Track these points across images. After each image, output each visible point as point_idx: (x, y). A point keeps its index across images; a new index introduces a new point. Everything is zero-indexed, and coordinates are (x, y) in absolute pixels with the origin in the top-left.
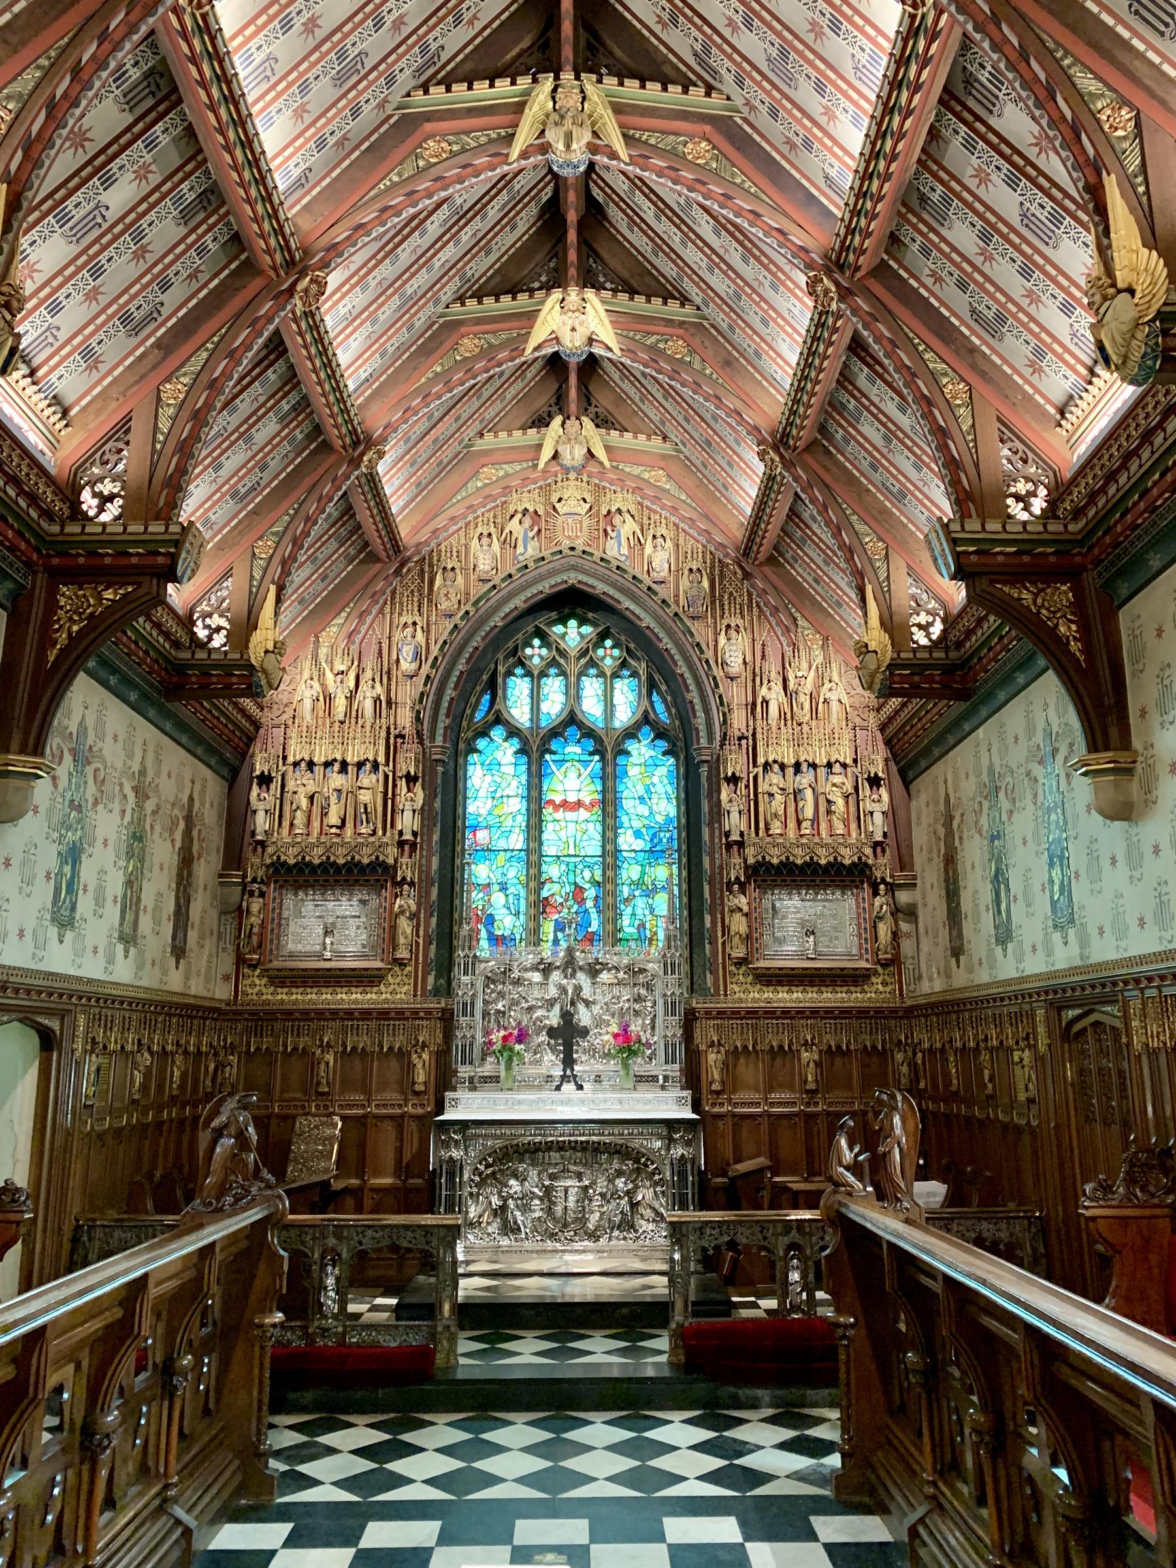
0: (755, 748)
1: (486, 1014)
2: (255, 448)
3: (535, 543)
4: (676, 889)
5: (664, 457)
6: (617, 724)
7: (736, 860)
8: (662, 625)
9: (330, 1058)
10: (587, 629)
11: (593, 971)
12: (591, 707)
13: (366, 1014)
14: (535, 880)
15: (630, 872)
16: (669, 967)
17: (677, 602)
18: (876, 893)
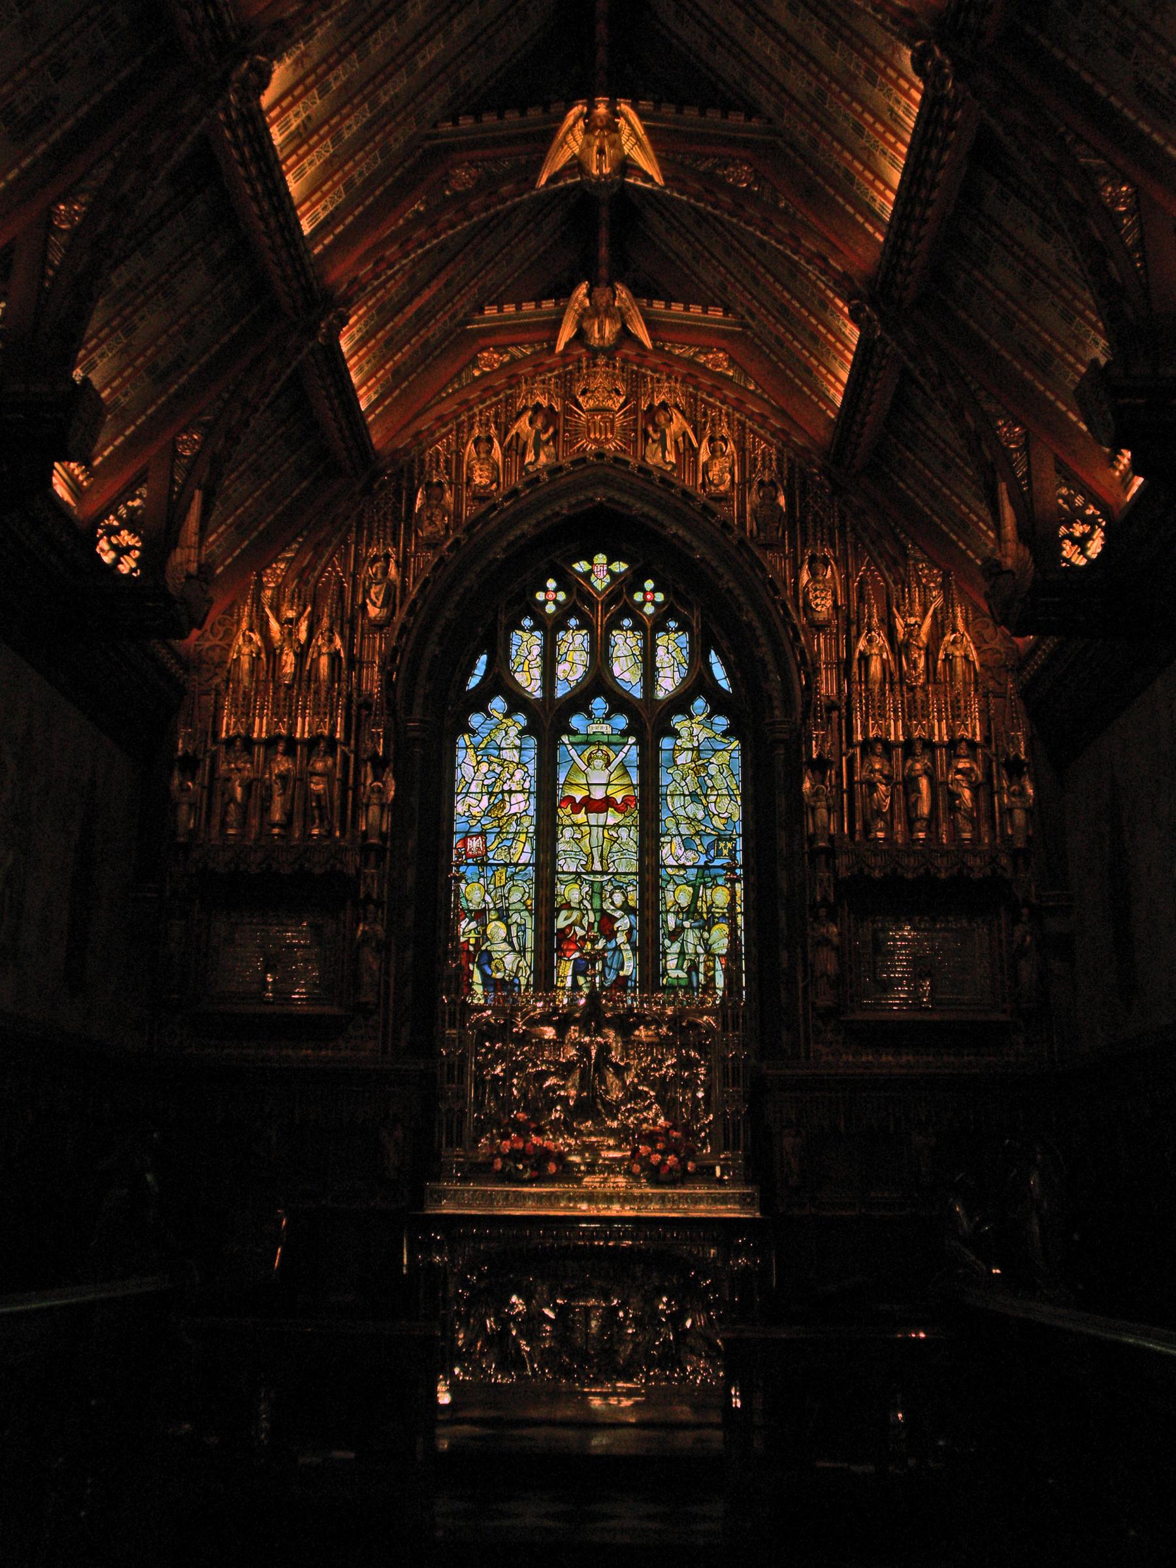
5: (725, 335)
6: (661, 694)
7: (824, 874)
10: (620, 567)
12: (625, 671)
14: (546, 904)
15: (678, 895)
17: (742, 525)
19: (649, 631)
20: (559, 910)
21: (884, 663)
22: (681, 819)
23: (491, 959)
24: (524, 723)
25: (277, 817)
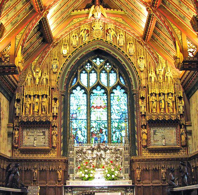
0: (148, 90)
1: (76, 161)
2: (17, 11)
3: (88, 38)
4: (127, 129)
8: (122, 58)
9: (36, 171)
10: (102, 61)
11: (105, 150)
12: (104, 81)
13: (45, 161)
14: (89, 127)
15: (115, 125)
16: (126, 149)
18: (181, 128)
19: (108, 73)
20: (91, 128)
21: (155, 78)
22: (115, 110)
23: (78, 138)
24: (84, 92)
25: (193, 59)
